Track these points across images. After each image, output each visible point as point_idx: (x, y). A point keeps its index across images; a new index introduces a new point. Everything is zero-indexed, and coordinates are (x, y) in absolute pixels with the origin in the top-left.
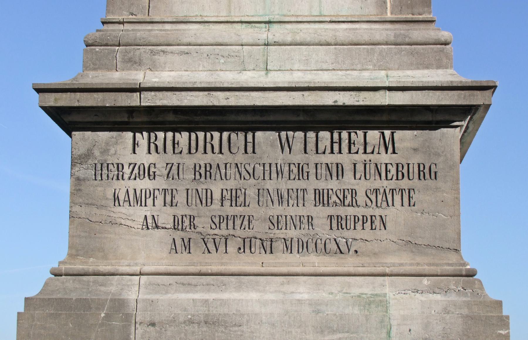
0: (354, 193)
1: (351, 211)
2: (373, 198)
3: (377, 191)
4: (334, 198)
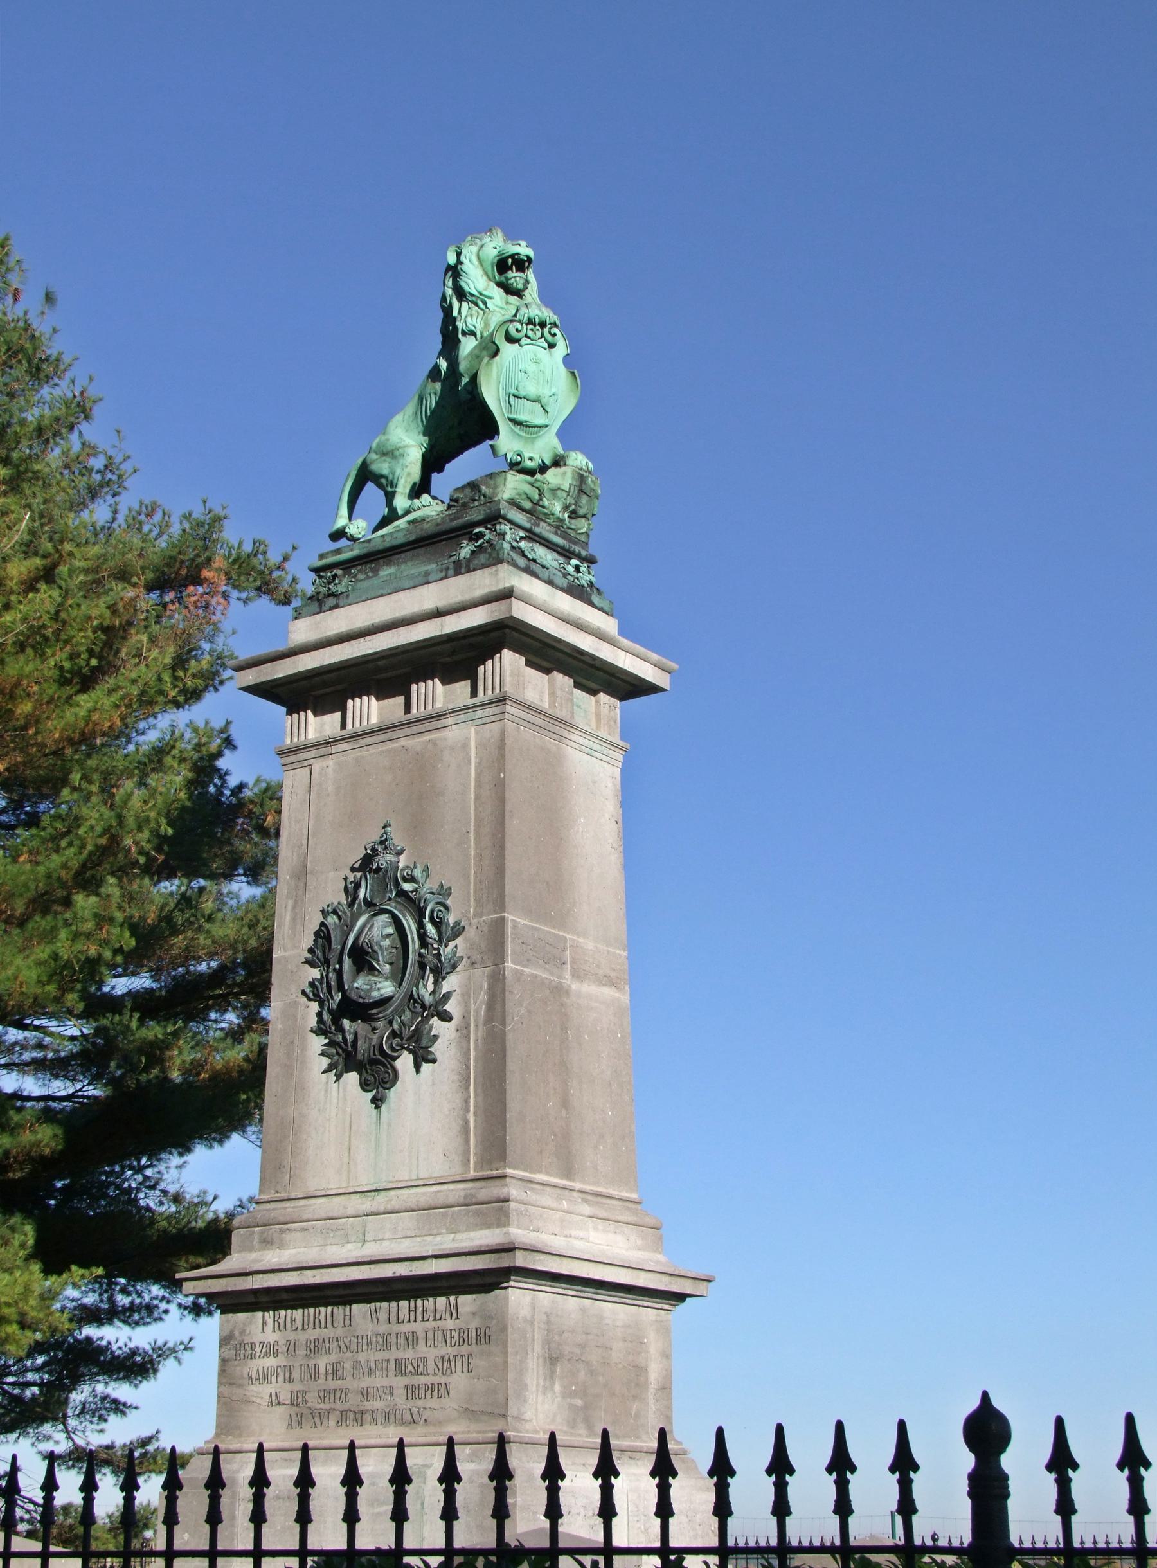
0: (425, 1360)
1: (423, 1380)
2: (440, 1365)
3: (443, 1357)
4: (410, 1368)
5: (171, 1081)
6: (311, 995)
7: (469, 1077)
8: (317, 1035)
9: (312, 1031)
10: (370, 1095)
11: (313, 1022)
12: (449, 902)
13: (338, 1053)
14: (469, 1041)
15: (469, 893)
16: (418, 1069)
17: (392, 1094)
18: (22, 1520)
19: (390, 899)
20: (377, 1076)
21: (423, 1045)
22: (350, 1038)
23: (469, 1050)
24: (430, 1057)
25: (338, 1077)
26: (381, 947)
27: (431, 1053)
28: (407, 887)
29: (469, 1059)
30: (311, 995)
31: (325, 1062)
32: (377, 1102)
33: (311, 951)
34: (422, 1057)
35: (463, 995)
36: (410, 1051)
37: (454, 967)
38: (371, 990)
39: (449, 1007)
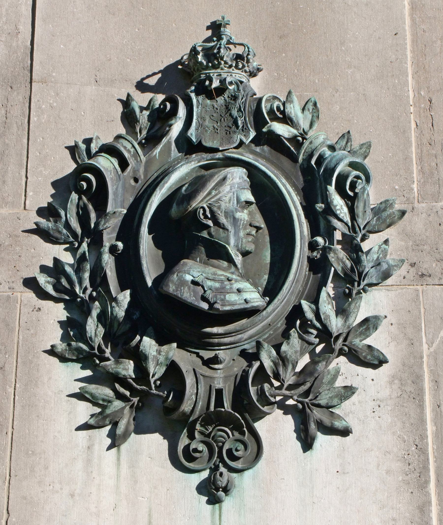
5: (195, 89)
6: (50, 289)
7: (426, 468)
10: (196, 479)
11: (54, 336)
12: (367, 163)
13: (120, 396)
14: (421, 406)
15: (407, 159)
16: (307, 443)
19: (241, 143)
21: (323, 401)
22: (156, 371)
23: (422, 421)
24: (338, 424)
25: (116, 441)
26: (235, 221)
27: (339, 417)
28: (281, 129)
29: (423, 437)
30: (50, 289)
31: (84, 411)
33: (48, 212)
35: (402, 326)
36: (287, 410)
37: (386, 275)
38: (222, 291)
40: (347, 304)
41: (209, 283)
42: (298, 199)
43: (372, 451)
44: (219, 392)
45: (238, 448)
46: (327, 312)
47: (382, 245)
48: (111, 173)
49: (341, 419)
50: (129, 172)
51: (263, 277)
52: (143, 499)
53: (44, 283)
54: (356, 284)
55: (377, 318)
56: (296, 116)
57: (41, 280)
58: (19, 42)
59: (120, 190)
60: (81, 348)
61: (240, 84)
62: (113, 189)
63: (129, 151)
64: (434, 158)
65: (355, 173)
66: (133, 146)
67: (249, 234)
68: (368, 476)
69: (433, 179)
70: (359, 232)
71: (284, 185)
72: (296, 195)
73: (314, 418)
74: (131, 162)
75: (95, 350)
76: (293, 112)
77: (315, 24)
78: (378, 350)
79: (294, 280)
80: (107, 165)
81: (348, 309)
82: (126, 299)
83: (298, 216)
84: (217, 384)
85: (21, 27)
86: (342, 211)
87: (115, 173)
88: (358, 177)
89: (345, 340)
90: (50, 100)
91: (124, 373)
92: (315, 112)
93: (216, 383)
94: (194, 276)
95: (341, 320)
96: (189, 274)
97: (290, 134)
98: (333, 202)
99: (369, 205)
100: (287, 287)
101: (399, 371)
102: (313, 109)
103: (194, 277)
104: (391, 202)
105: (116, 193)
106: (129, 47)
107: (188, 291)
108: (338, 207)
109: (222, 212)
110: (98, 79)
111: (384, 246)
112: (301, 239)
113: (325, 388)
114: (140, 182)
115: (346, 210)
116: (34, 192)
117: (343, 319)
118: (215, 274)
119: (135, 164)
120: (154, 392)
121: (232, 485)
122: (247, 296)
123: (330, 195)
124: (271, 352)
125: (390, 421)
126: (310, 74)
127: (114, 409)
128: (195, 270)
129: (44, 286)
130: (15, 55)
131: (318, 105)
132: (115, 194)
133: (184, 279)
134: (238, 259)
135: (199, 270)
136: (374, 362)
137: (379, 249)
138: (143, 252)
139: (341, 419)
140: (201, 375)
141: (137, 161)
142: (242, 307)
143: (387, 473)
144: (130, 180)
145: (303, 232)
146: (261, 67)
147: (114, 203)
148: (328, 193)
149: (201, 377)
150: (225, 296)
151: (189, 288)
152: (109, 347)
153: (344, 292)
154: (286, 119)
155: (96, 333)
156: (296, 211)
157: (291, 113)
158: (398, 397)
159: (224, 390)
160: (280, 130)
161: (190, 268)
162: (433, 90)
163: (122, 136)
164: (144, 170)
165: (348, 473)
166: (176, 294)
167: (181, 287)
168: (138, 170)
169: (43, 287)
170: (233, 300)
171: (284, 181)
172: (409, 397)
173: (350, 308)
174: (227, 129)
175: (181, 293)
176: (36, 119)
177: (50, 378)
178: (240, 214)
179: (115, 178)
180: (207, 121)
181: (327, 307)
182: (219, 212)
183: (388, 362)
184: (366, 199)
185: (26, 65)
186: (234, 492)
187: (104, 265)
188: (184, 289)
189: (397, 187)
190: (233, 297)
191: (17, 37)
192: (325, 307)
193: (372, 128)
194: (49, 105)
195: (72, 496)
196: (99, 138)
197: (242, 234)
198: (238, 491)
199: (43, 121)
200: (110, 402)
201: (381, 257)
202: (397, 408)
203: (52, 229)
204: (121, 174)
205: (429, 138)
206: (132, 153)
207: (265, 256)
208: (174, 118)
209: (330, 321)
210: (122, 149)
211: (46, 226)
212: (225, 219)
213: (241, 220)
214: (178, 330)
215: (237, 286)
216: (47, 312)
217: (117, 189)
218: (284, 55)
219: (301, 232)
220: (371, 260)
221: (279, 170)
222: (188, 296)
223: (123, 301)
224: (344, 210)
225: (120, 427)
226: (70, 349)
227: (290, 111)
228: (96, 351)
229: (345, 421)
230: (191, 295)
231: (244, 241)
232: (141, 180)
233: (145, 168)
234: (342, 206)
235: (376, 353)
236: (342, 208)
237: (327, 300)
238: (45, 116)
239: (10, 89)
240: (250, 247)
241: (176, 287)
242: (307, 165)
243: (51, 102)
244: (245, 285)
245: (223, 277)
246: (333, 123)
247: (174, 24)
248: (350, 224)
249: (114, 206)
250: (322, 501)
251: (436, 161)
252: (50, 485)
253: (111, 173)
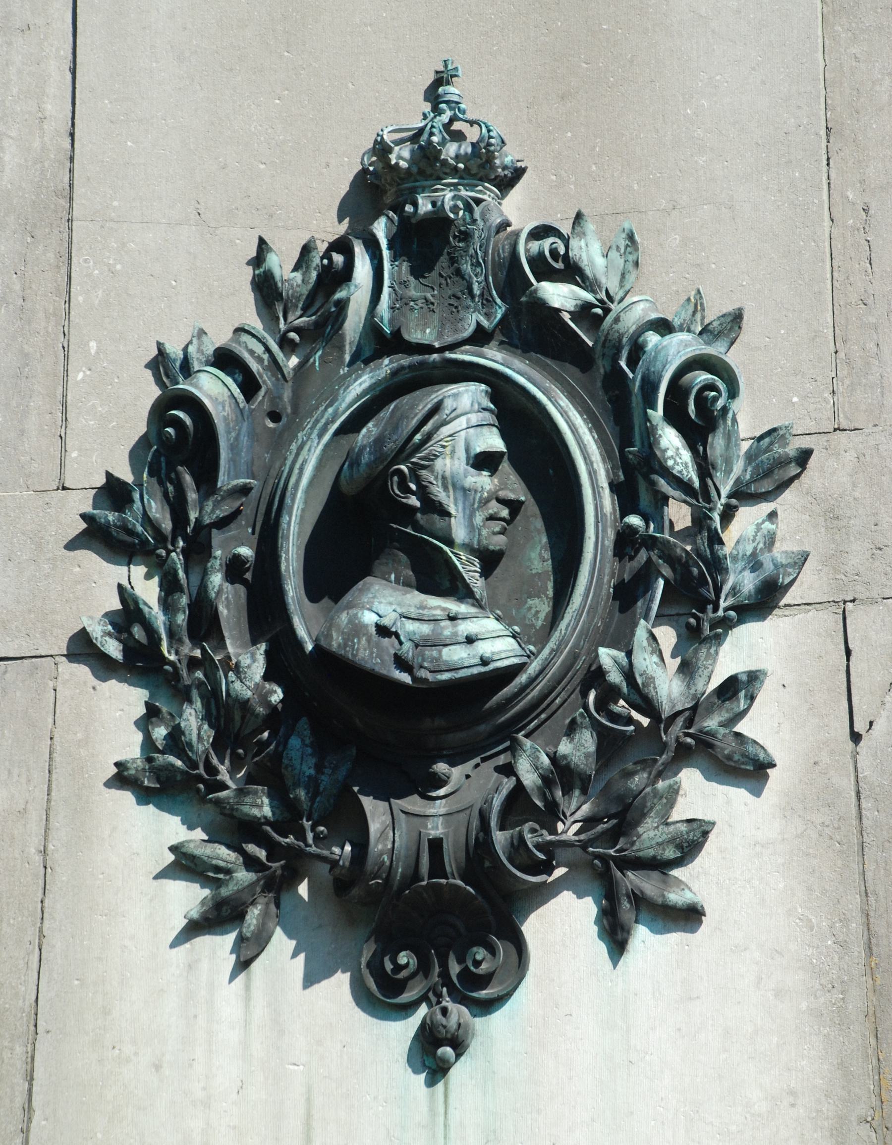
8: (145, 796)
9: (122, 778)
12: (734, 358)
16: (616, 937)
17: (494, 1032)
18: (248, 688)
20: (435, 949)
28: (559, 295)
32: (435, 1053)
33: (114, 492)
34: (636, 892)
39: (760, 725)
40: (691, 650)
41: (411, 626)
42: (593, 437)
43: (745, 949)
44: (436, 845)
45: (479, 957)
46: (650, 671)
47: (763, 522)
48: (224, 407)
49: (683, 887)
50: (262, 402)
51: (526, 602)
52: (296, 1068)
53: (102, 637)
54: (710, 607)
55: (754, 677)
56: (592, 263)
57: (94, 631)
58: (45, 139)
59: (244, 440)
60: (173, 766)
61: (474, 205)
62: (229, 440)
63: (259, 360)
64: (873, 331)
65: (705, 380)
66: (268, 350)
67: (492, 518)
68: (739, 1003)
69: (869, 377)
70: (716, 497)
71: (564, 413)
72: (590, 430)
73: (626, 886)
74: (264, 382)
75: (198, 769)
76: (584, 257)
77: (631, 62)
78: (755, 742)
79: (584, 607)
80: (216, 392)
81: (694, 660)
82: (256, 664)
83: (592, 474)
84: (433, 828)
85: (49, 107)
86: (679, 460)
87: (233, 406)
88: (712, 387)
89: (690, 723)
90: (109, 258)
91: (255, 812)
92: (630, 253)
93: (430, 826)
94: (380, 613)
95: (679, 683)
96: (370, 610)
97: (579, 302)
98: (659, 443)
99: (736, 440)
100: (569, 624)
101: (800, 781)
102: (627, 246)
103: (380, 617)
104: (781, 432)
105: (237, 446)
106: (262, 138)
107: (366, 646)
108: (669, 453)
109: (436, 478)
110: (203, 210)
111: (768, 525)
112: (597, 522)
113: (649, 825)
114: (284, 420)
115: (686, 456)
116: (80, 450)
117: (683, 682)
118: (423, 607)
119: (273, 384)
120: (313, 849)
121: (466, 1032)
122: (485, 648)
123: (653, 429)
124: (538, 758)
125: (781, 886)
126: (622, 172)
127: (235, 888)
128: (384, 601)
129: (101, 643)
130: (38, 166)
131: (637, 237)
132: (234, 447)
133: (360, 622)
134: (469, 570)
135: (391, 599)
136: (748, 768)
137: (756, 533)
138: (288, 567)
139: (683, 887)
140: (402, 811)
141: (277, 379)
142: (475, 671)
143: (776, 995)
144: (264, 419)
145: (602, 508)
146: (523, 165)
147: (232, 468)
148: (648, 424)
149: (403, 816)
150: (440, 652)
151: (369, 641)
152: (227, 762)
153: (688, 625)
154: (572, 272)
155: (199, 734)
156: (586, 464)
157: (580, 258)
158: (797, 836)
159: (444, 841)
160: (555, 297)
161: (374, 597)
162: (873, 186)
163: (246, 328)
164: (291, 395)
165: (698, 997)
166: (343, 652)
167: (354, 637)
168: (280, 397)
169: (99, 645)
170: (455, 658)
171: (564, 402)
172: (821, 835)
173: (698, 659)
174: (452, 301)
175: (353, 649)
176: (81, 299)
177: (114, 829)
178: (473, 479)
179: (232, 416)
180: (412, 288)
181: (648, 660)
182: (432, 479)
183: (775, 765)
184: (731, 428)
185: (59, 187)
186: (475, 1046)
187: (213, 595)
188: (359, 642)
189: (795, 399)
190: (457, 654)
191: (41, 128)
192: (645, 659)
193: (746, 277)
194: (106, 268)
195: (157, 1067)
196: (206, 333)
197: (479, 519)
198: (481, 1043)
199: (97, 302)
200: (228, 872)
201: (761, 549)
202: (795, 858)
203: (115, 525)
204: (244, 407)
205: (863, 290)
206: (266, 363)
207: (530, 560)
208: (344, 286)
209: (655, 688)
210: (246, 356)
211: (103, 520)
212: (444, 491)
213: (476, 491)
214: (357, 721)
215: (466, 628)
216: (108, 694)
217: (237, 439)
218: (569, 134)
219: (598, 507)
220: (740, 555)
221: (556, 380)
222: (371, 656)
223: (249, 667)
224: (683, 457)
225: (249, 922)
226: (152, 770)
227: (578, 256)
228: (201, 771)
229: (690, 889)
230: (371, 653)
231: (484, 532)
232: (287, 416)
233: (293, 392)
234: (678, 449)
235: (751, 749)
236: (677, 455)
237: (650, 645)
238: (100, 292)
239: (29, 239)
240: (499, 542)
241: (343, 639)
242: (612, 366)
243: (111, 262)
244: (488, 625)
245: (438, 612)
246: (667, 273)
247: (350, 85)
248: (697, 484)
249: (232, 473)
250: (647, 1057)
251: (876, 338)
252: (114, 1048)
253: (224, 407)
